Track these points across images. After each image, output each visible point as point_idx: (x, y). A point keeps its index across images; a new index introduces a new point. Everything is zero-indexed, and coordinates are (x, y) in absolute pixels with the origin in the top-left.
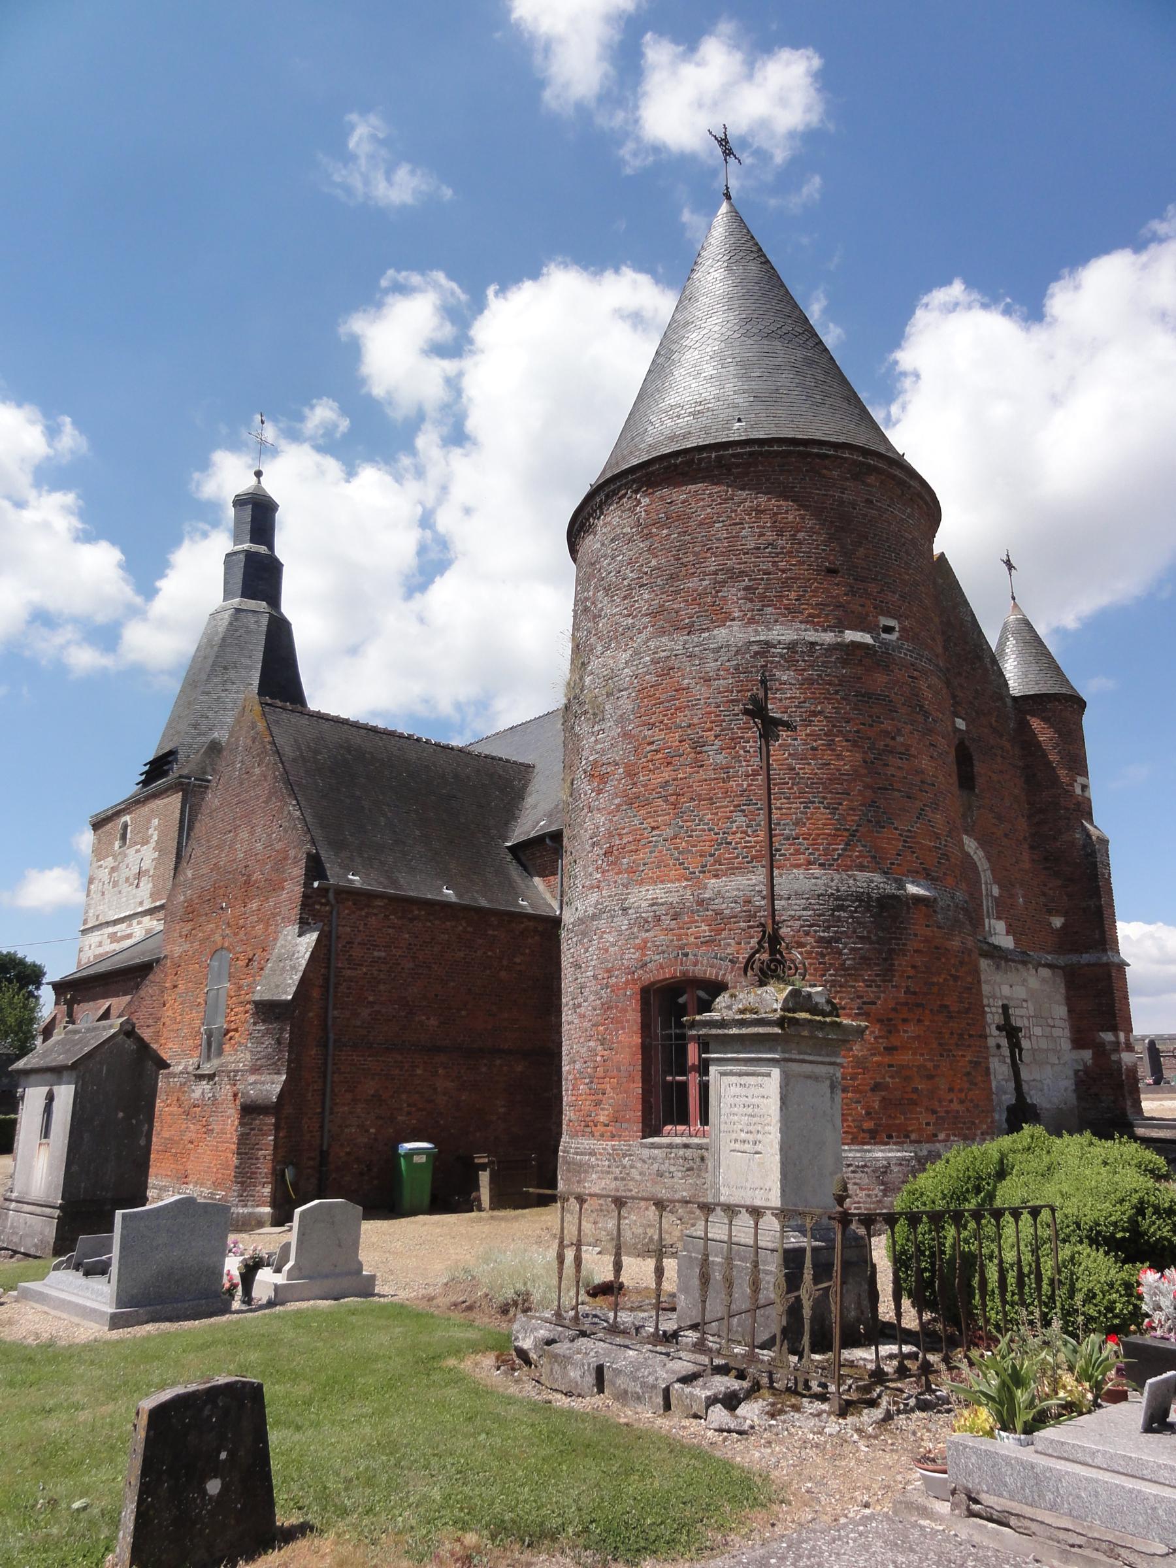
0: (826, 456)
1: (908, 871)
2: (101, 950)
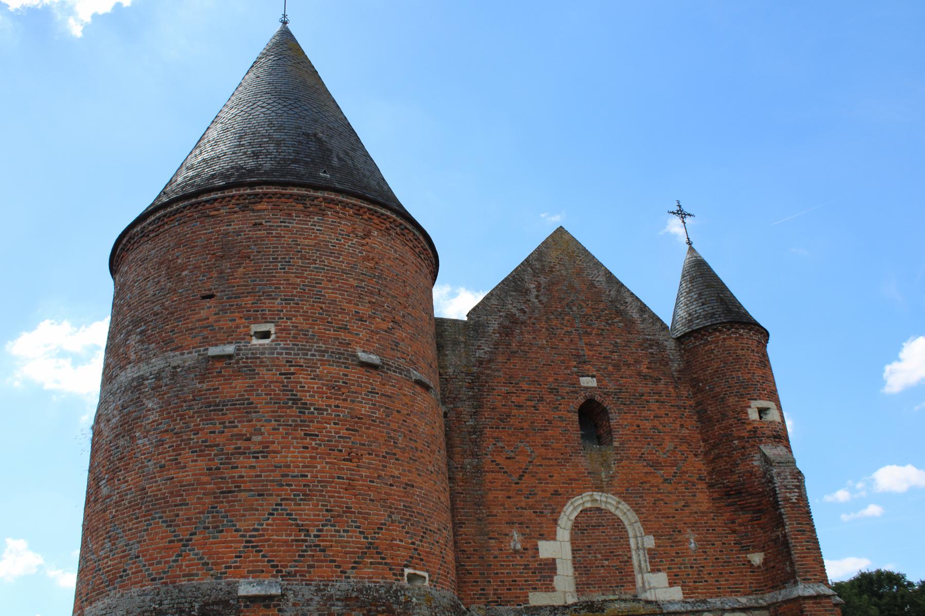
0: (215, 200)
1: (249, 572)
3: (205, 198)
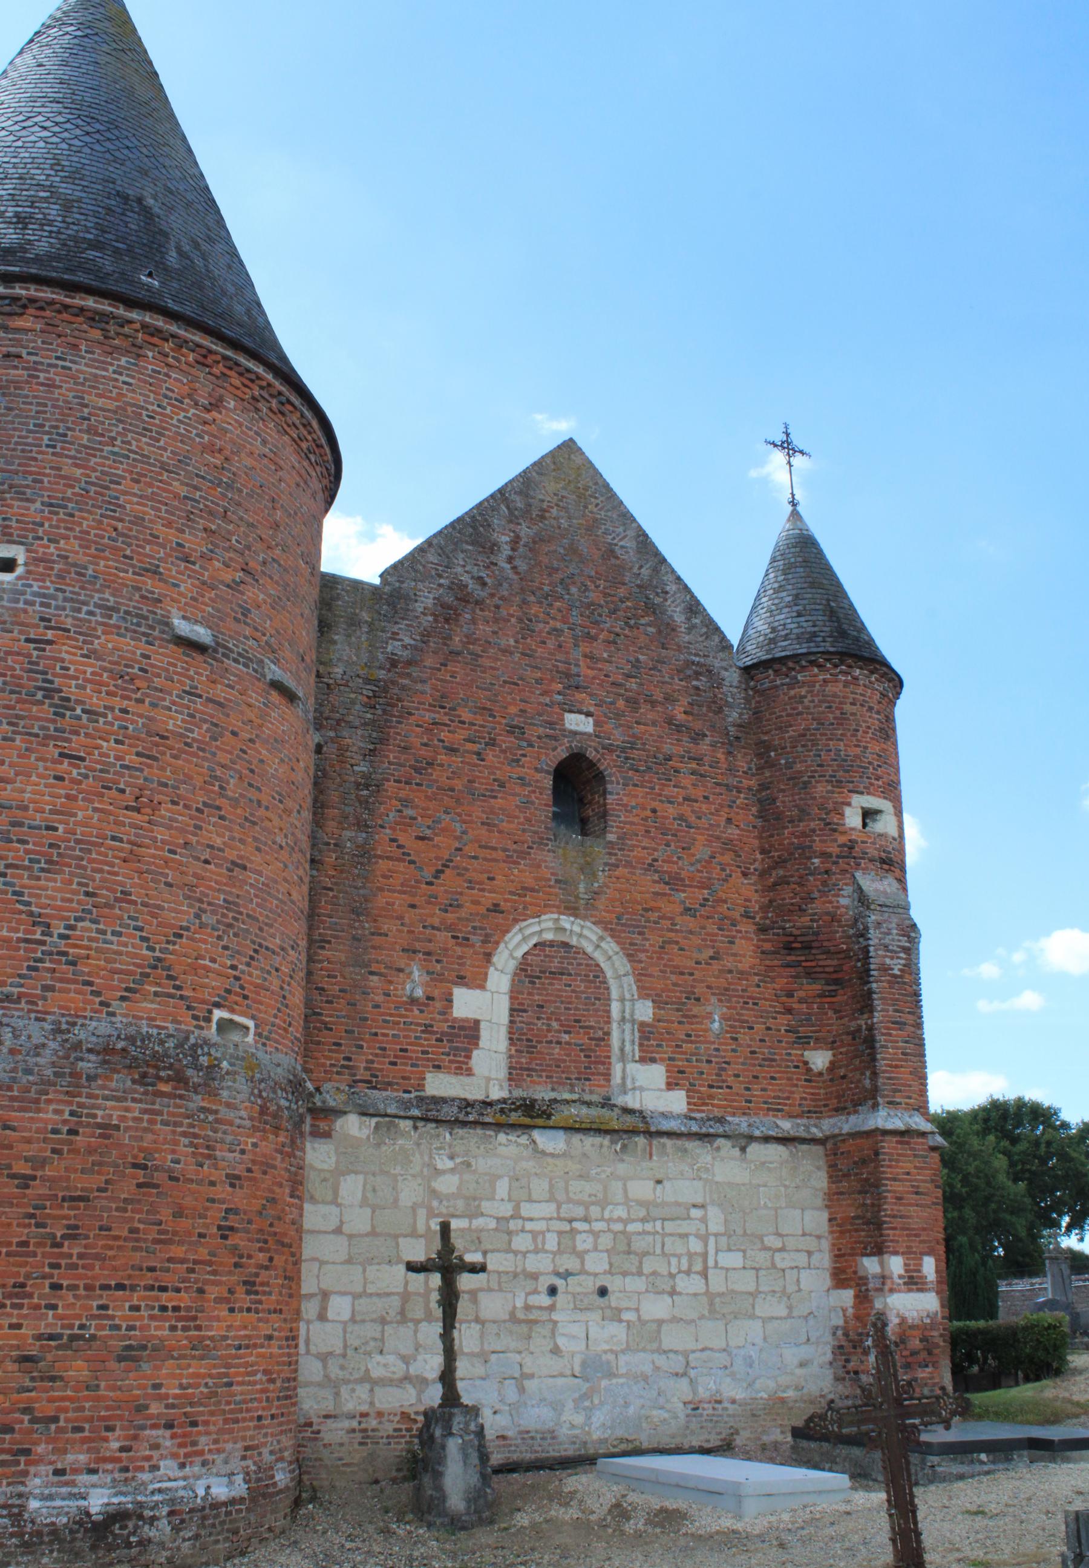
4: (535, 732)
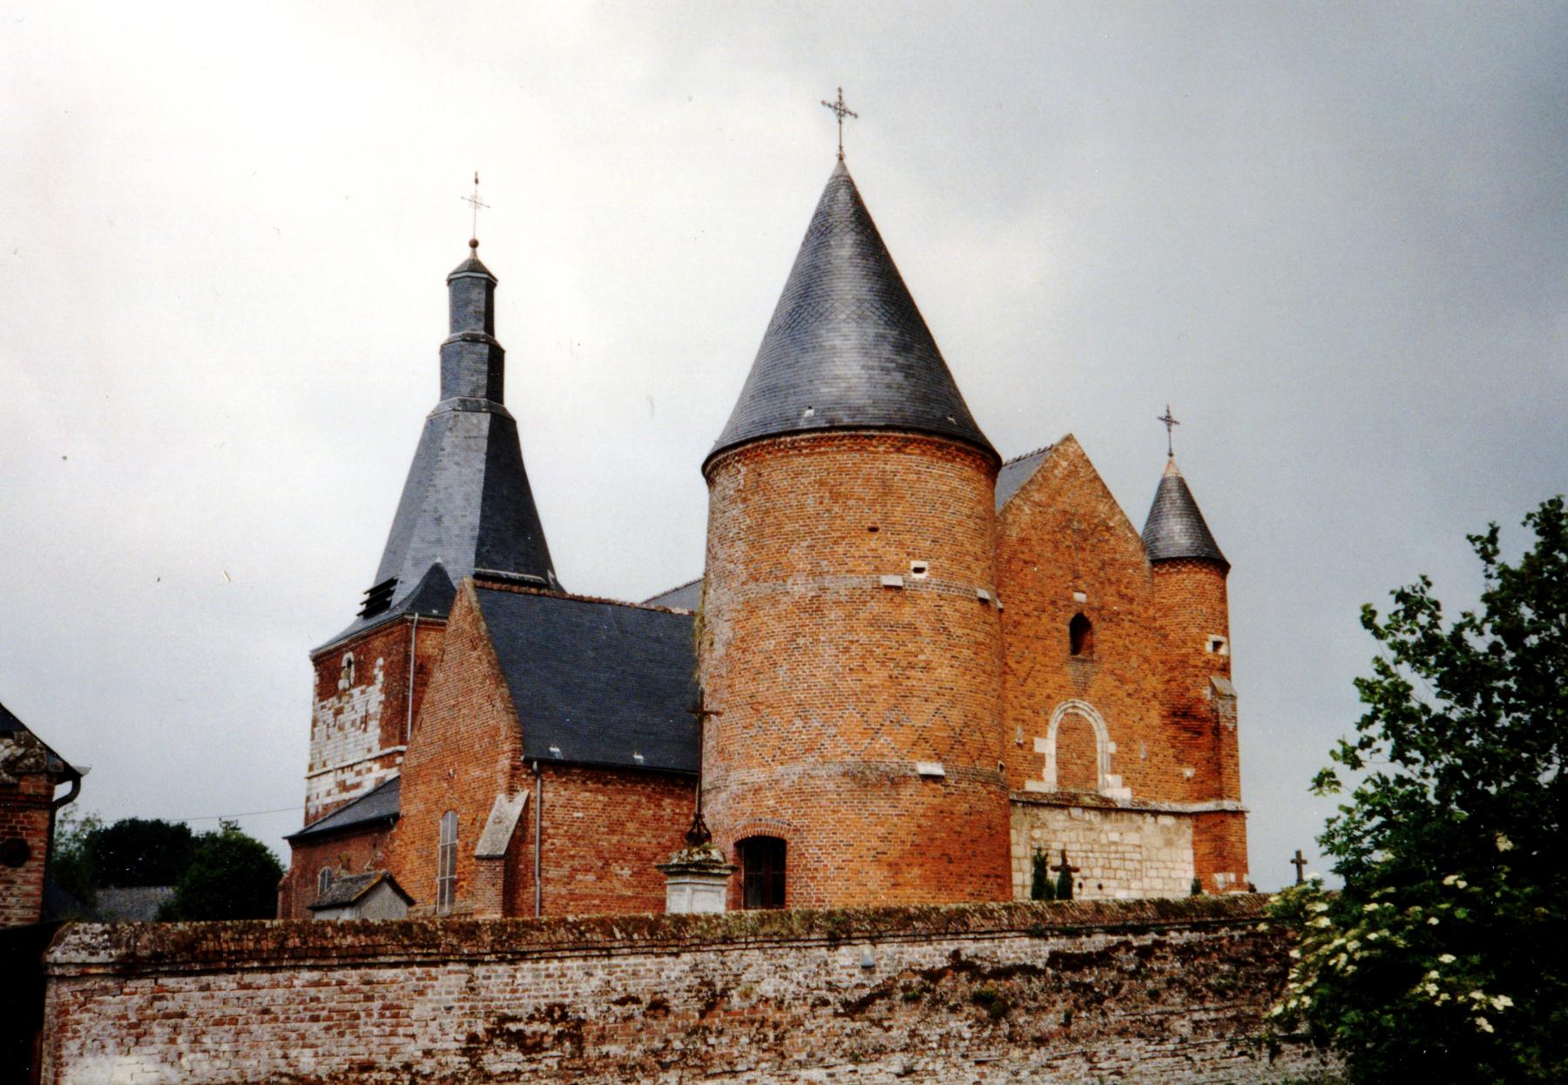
2: (329, 800)
3: (864, 433)
4: (1061, 603)
